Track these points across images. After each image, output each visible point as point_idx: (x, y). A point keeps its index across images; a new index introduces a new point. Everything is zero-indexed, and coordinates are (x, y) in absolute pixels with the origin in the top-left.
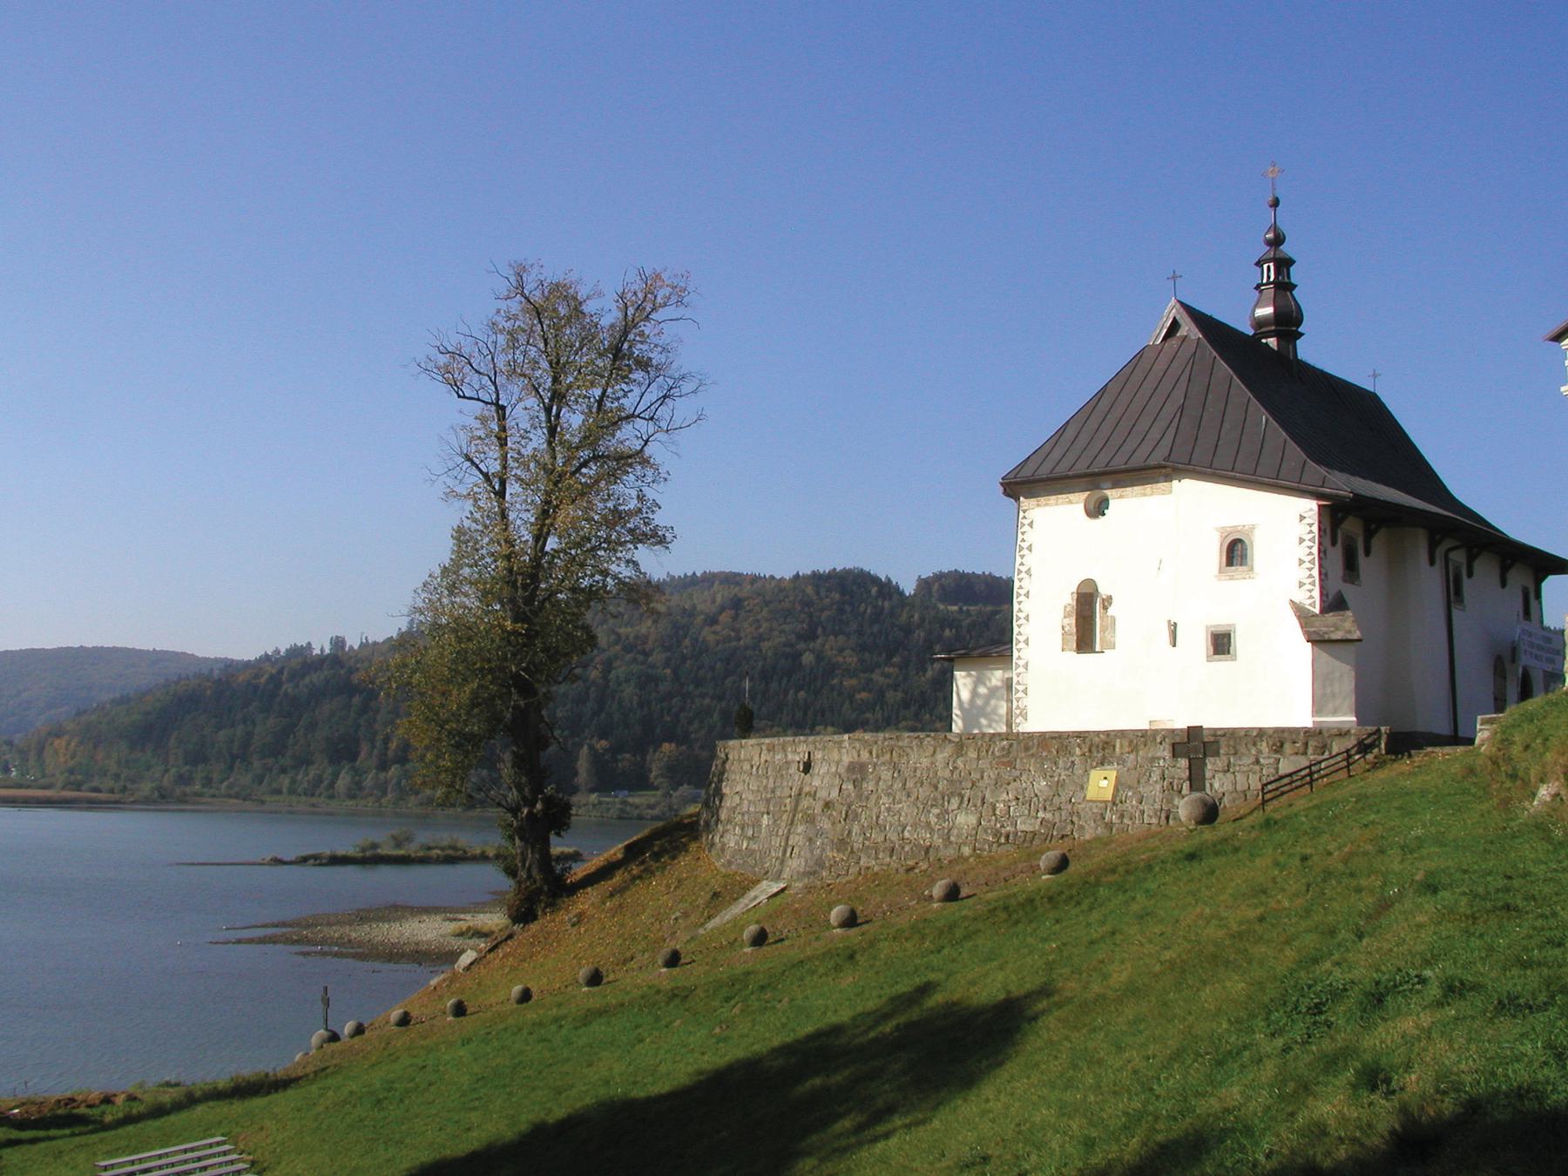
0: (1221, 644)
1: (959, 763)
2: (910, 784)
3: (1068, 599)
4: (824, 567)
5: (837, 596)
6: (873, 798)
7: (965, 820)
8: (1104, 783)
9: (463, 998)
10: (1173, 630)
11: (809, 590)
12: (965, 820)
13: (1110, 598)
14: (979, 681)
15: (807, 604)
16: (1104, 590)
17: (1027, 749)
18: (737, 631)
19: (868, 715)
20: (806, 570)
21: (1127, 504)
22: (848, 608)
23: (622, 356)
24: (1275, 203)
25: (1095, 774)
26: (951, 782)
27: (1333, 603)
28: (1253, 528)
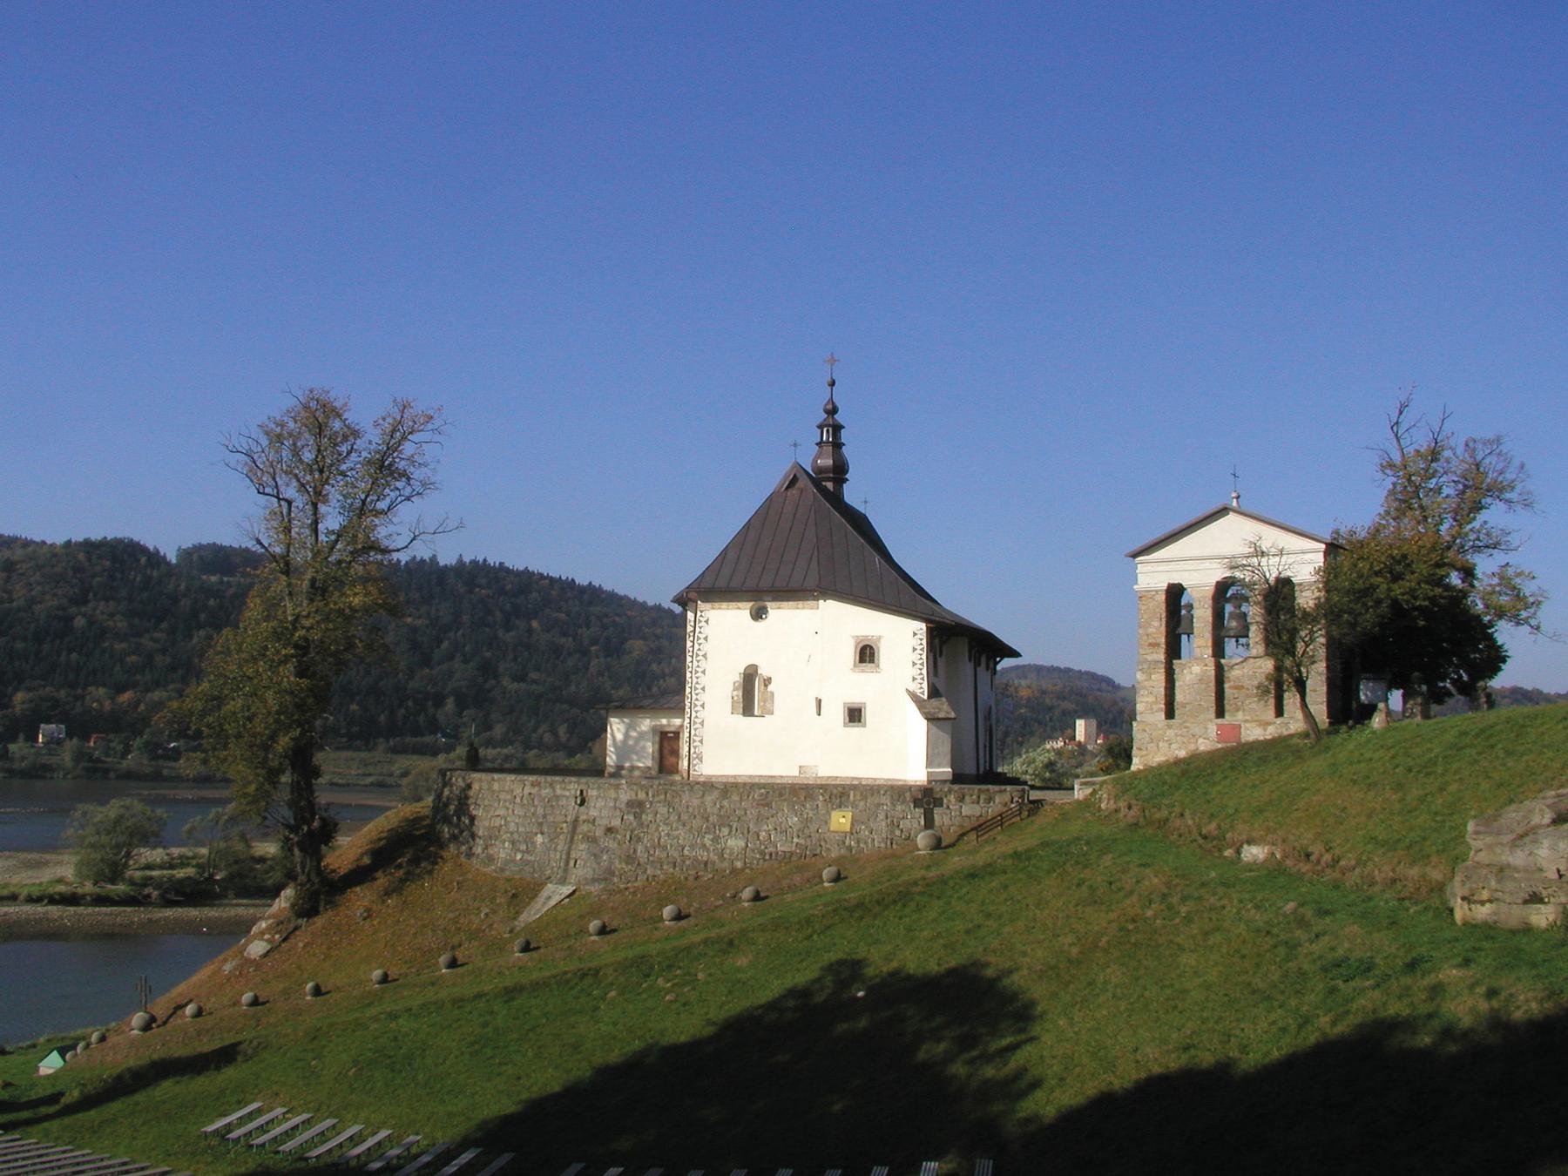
0: (855, 715)
1: (725, 803)
2: (685, 817)
3: (736, 676)
4: (96, 536)
5: (108, 564)
6: (653, 826)
7: (735, 843)
8: (842, 820)
9: (319, 981)
10: (819, 702)
11: (81, 556)
12: (735, 843)
13: (769, 679)
14: (630, 727)
15: (78, 569)
17: (781, 795)
18: (10, 592)
19: (138, 677)
20: (78, 537)
21: (782, 615)
22: (118, 575)
23: (385, 468)
24: (833, 384)
26: (720, 817)
27: (934, 692)
28: (880, 638)
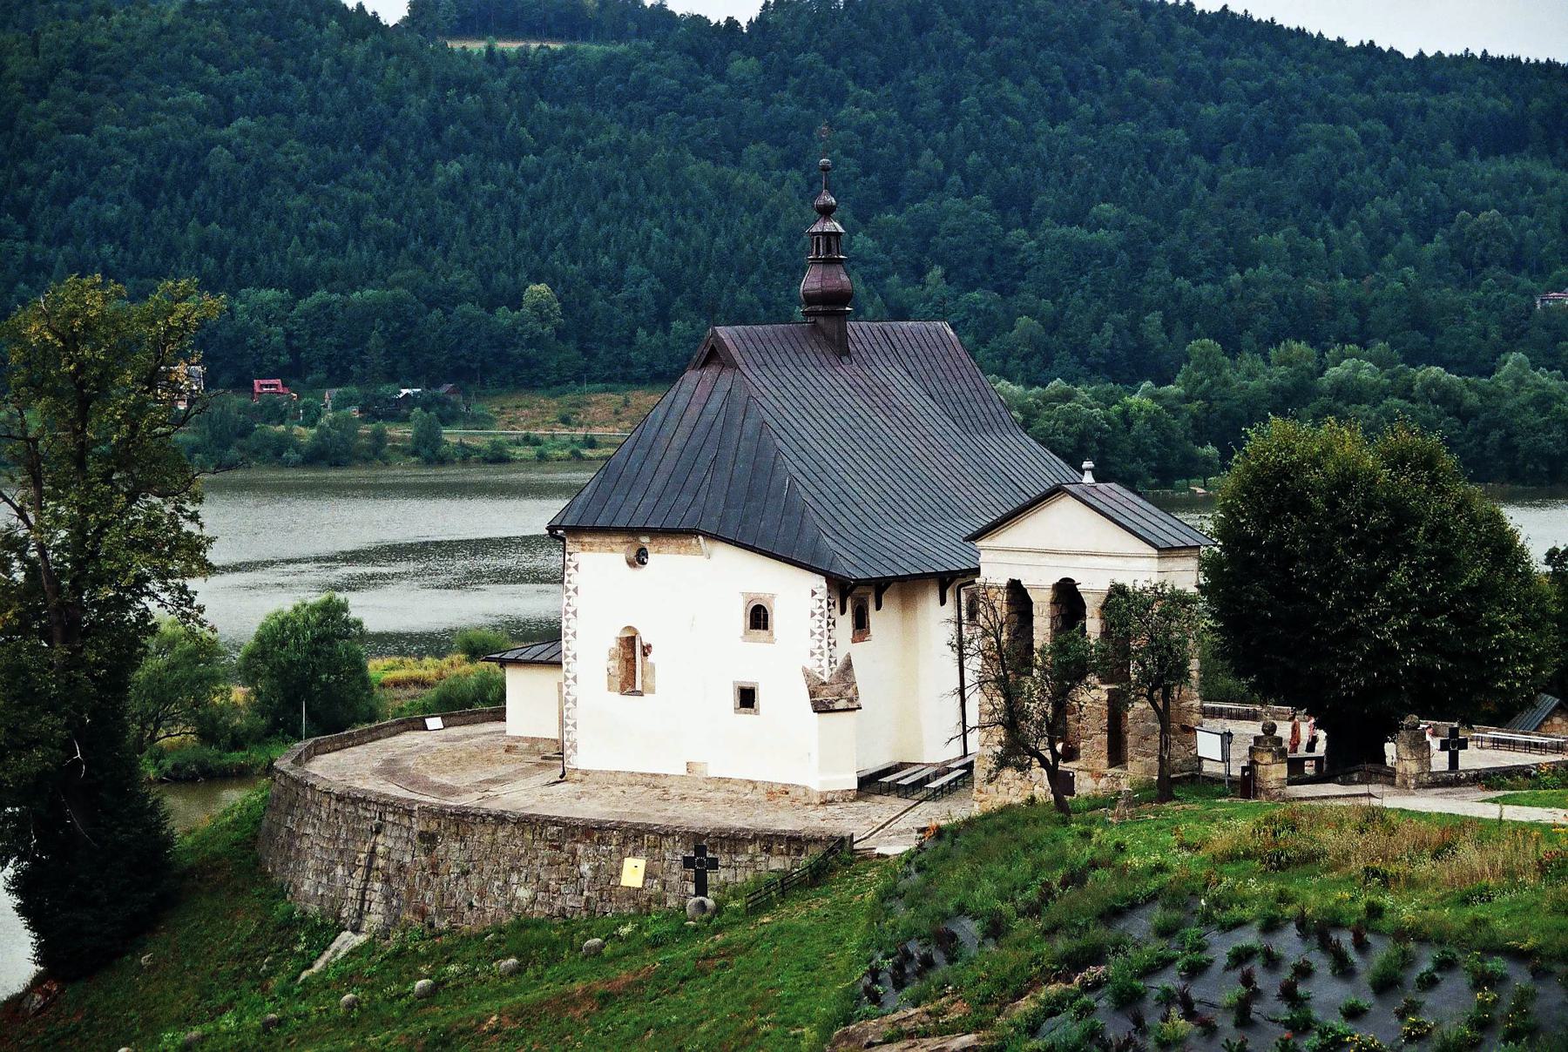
16: (645, 637)
21: (666, 561)
25: (629, 863)
28: (773, 596)
